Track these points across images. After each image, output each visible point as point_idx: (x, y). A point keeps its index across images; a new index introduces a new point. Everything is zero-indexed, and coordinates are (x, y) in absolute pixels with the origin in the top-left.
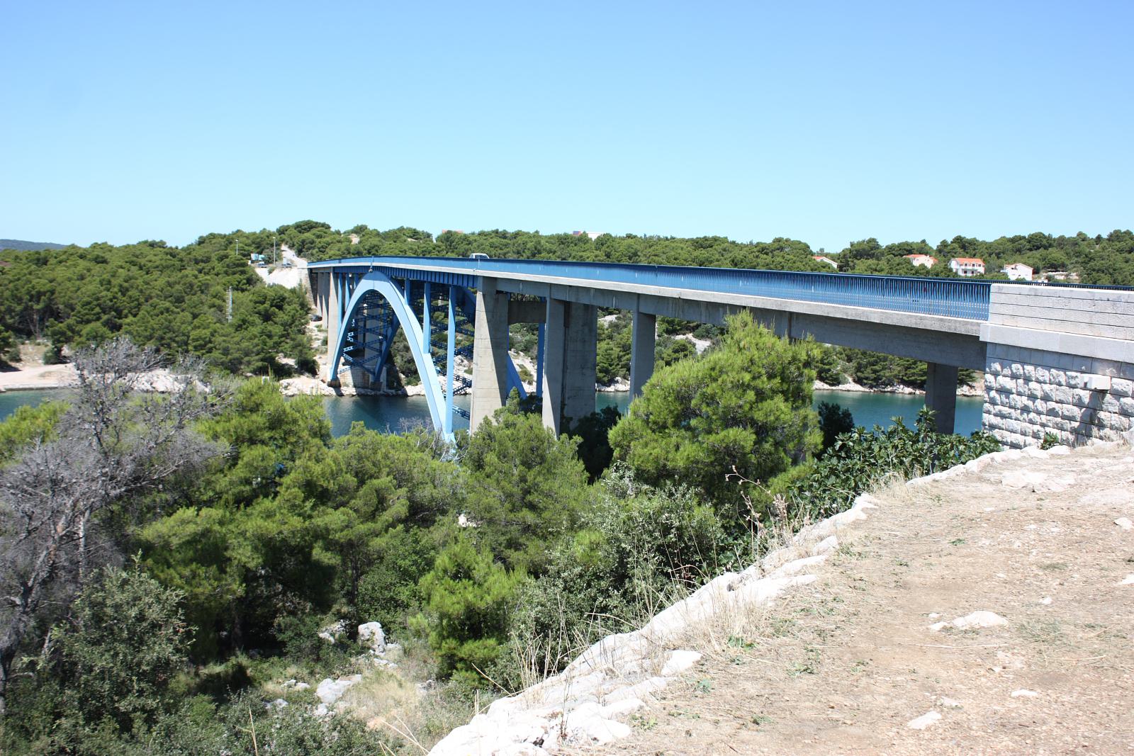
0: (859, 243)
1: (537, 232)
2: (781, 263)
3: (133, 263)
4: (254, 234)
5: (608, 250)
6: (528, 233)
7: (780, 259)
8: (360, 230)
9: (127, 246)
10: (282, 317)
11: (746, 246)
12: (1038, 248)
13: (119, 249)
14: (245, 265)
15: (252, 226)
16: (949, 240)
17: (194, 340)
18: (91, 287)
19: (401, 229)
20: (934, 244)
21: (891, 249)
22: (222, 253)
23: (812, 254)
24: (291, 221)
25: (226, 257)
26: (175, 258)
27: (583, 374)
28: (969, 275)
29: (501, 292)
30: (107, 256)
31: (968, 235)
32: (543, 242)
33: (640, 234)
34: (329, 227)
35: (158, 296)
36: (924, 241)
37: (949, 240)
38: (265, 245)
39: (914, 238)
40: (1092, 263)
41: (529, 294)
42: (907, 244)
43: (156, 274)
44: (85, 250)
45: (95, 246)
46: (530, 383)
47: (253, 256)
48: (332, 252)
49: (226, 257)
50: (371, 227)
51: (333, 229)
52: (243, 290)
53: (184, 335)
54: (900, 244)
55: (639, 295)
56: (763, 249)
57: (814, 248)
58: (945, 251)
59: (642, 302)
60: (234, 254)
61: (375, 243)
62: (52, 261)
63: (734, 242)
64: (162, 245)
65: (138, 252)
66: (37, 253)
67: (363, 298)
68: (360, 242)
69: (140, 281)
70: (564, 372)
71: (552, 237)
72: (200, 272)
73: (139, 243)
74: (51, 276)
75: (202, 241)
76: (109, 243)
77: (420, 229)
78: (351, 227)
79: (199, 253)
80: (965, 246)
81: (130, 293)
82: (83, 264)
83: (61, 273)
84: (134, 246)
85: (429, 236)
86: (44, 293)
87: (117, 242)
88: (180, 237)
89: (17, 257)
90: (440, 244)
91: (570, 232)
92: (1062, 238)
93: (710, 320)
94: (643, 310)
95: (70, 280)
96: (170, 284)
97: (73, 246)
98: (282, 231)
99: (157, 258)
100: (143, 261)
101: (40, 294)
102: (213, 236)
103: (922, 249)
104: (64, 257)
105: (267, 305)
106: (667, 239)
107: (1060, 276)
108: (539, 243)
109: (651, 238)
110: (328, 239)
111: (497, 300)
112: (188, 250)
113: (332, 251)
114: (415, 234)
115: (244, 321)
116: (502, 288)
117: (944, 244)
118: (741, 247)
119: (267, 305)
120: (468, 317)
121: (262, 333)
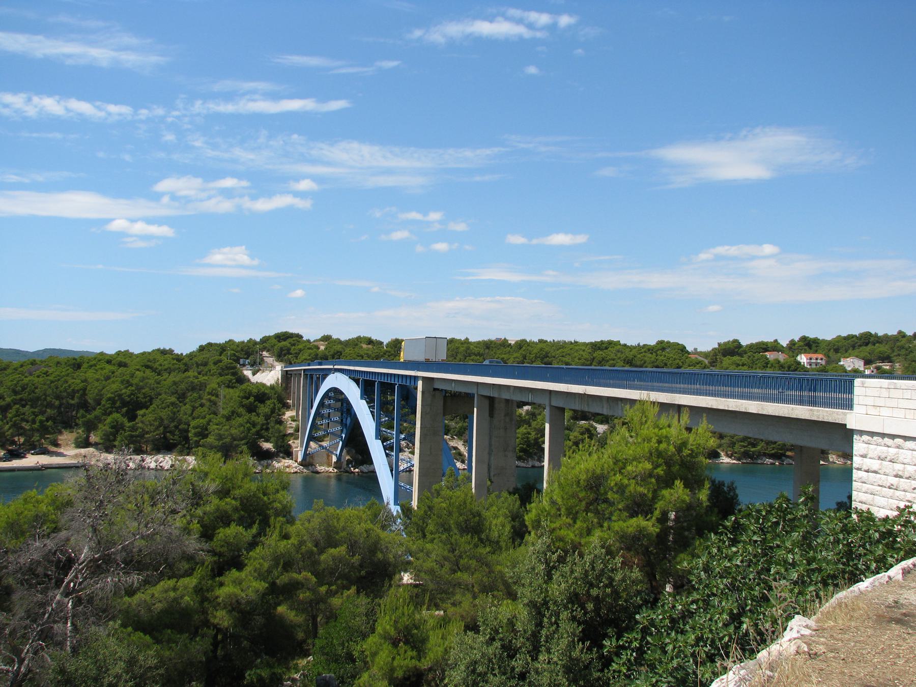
0: (725, 343)
1: (467, 339)
2: (663, 362)
3: (147, 367)
4: (243, 342)
7: (662, 358)
8: (327, 338)
9: (144, 354)
11: (635, 347)
12: (867, 344)
13: (137, 356)
14: (235, 368)
15: (241, 336)
16: (796, 339)
17: (194, 428)
18: (114, 386)
19: (359, 338)
20: (784, 343)
21: (751, 346)
22: (217, 358)
23: (688, 352)
25: (220, 361)
26: (181, 363)
27: (506, 456)
28: (814, 366)
29: (438, 389)
30: (127, 361)
31: (811, 335)
32: (472, 347)
34: (302, 337)
35: (166, 393)
36: (776, 341)
37: (796, 339)
38: (251, 352)
39: (769, 339)
40: (911, 355)
41: (463, 390)
42: (762, 343)
43: (165, 375)
44: (111, 356)
45: (119, 353)
46: (463, 462)
47: (241, 361)
49: (220, 361)
50: (334, 337)
51: (304, 339)
52: (233, 388)
53: (185, 424)
54: (757, 343)
55: (550, 391)
56: (649, 349)
57: (690, 348)
58: (794, 348)
60: (226, 360)
62: (85, 365)
63: (625, 345)
64: (171, 352)
65: (151, 358)
66: (75, 359)
67: (326, 395)
69: (151, 381)
71: (479, 343)
72: (199, 373)
73: (153, 351)
74: (83, 378)
75: (202, 349)
76: (131, 351)
77: (374, 338)
79: (200, 359)
80: (809, 344)
81: (143, 391)
82: (109, 367)
83: (90, 374)
84: (149, 353)
85: (382, 343)
86: (78, 391)
87: (136, 350)
88: (185, 346)
89: (58, 363)
90: (389, 349)
91: (493, 338)
92: (886, 336)
93: (609, 412)
94: (554, 404)
95: (98, 380)
96: (175, 383)
97: (102, 354)
98: (265, 340)
99: (166, 362)
100: (156, 365)
101: (74, 392)
102: (210, 344)
103: (775, 347)
104: (94, 362)
105: (252, 399)
106: (571, 343)
107: (886, 366)
108: (468, 348)
109: (559, 342)
110: (300, 347)
111: (434, 396)
112: (191, 356)
113: (302, 357)
114: (370, 341)
115: (233, 412)
117: (792, 343)
118: (631, 348)
119: (252, 399)
121: (248, 422)
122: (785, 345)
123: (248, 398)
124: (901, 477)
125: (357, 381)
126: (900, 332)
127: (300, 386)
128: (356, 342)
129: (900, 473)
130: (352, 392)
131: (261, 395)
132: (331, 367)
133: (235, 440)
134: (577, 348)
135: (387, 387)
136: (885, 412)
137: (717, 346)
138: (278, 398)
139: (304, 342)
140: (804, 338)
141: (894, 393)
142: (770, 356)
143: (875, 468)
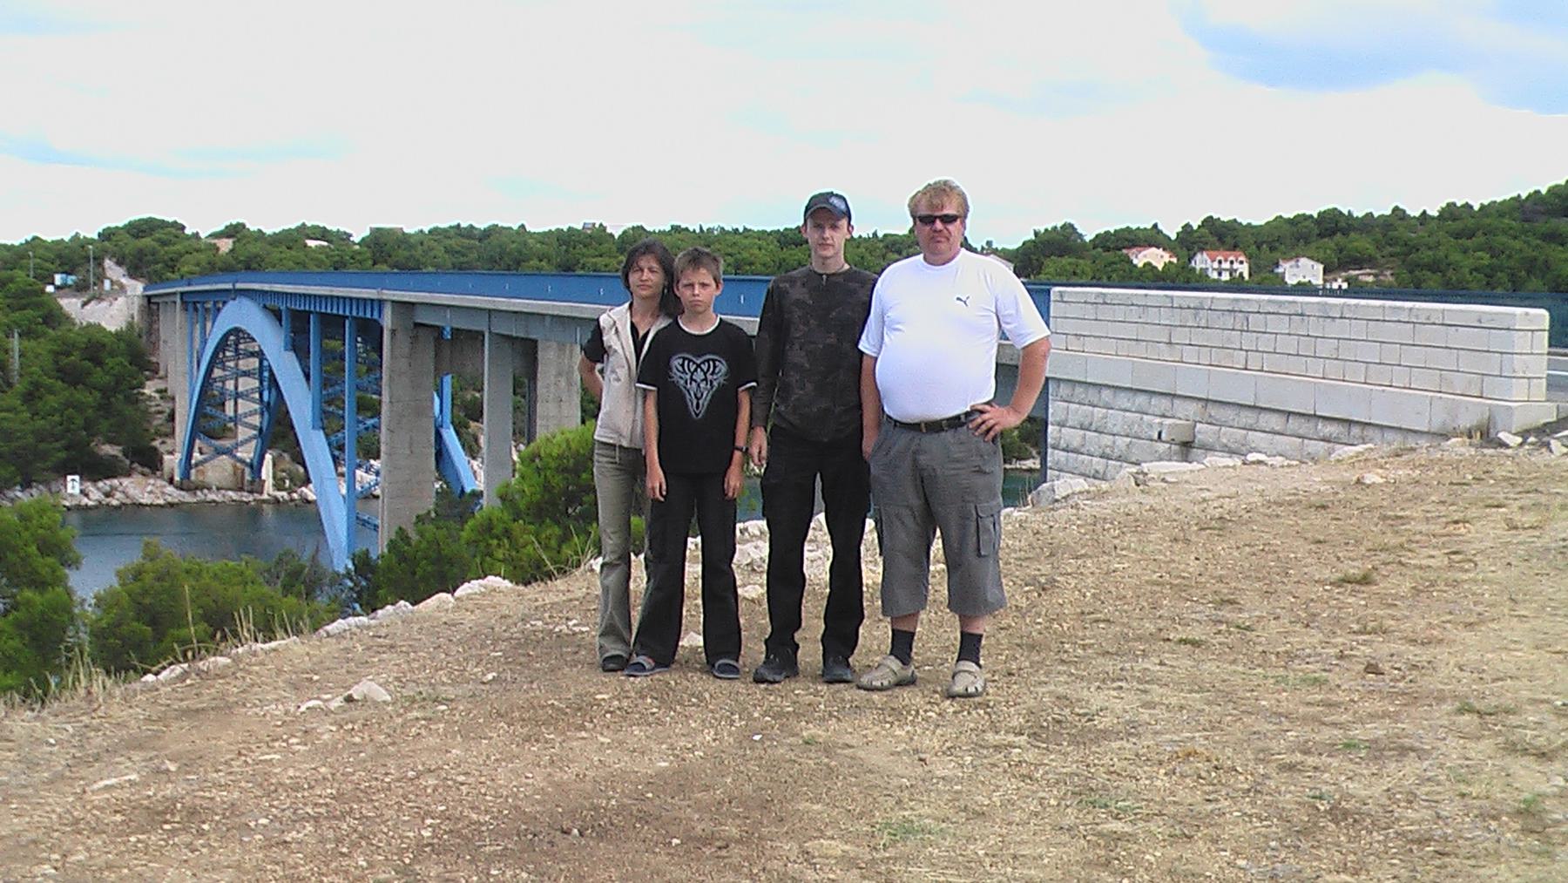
8: (234, 231)
15: (56, 231)
38: (77, 261)
51: (188, 231)
98: (107, 235)
103: (1153, 238)
111: (415, 339)
114: (323, 234)
122: (1088, 239)
123: (68, 354)
124: (1109, 458)
125: (277, 315)
126: (1396, 209)
127: (173, 328)
128: (292, 239)
129: (1108, 451)
130: (270, 338)
131: (96, 346)
132: (229, 286)
133: (42, 441)
134: (746, 242)
135: (332, 324)
136: (1090, 345)
137: (515, 227)
138: (136, 354)
139: (188, 238)
140: (1209, 222)
141: (1106, 312)
142: (1141, 258)
143: (1075, 444)
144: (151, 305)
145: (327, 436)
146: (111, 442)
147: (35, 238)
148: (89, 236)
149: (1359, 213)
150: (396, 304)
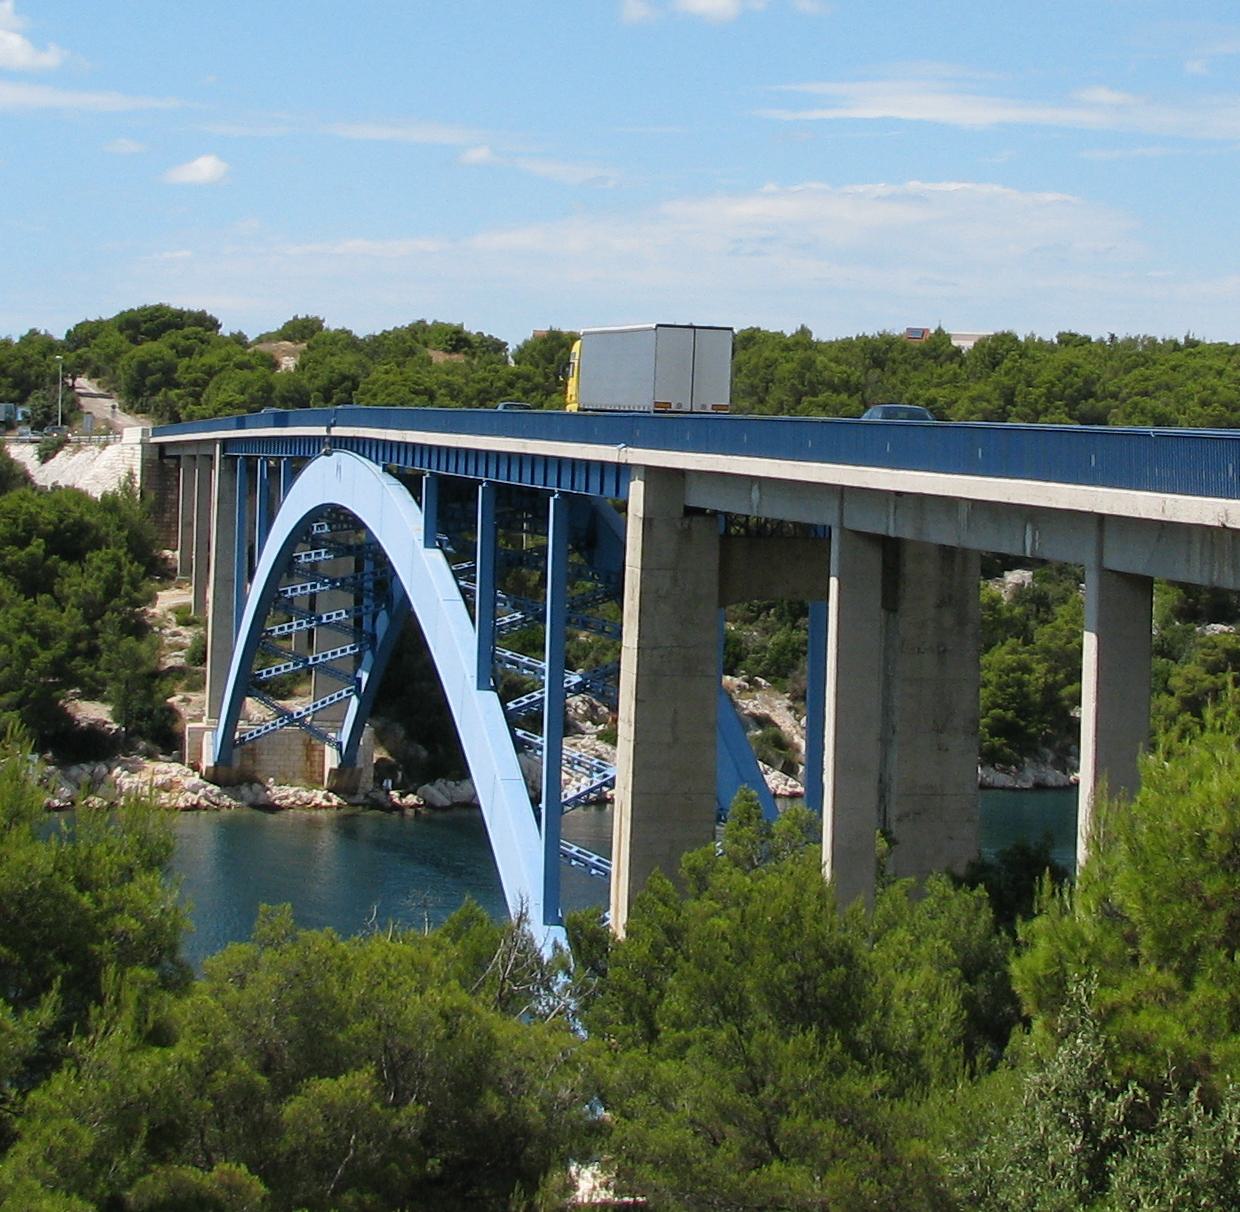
1: (804, 332)
5: (1006, 380)
6: (781, 335)
8: (303, 330)
10: (80, 581)
19: (418, 330)
24: (107, 309)
29: (700, 512)
32: (820, 359)
33: (1097, 332)
34: (214, 325)
46: (789, 769)
48: (222, 397)
50: (332, 324)
51: (225, 331)
59: (1110, 544)
61: (345, 368)
67: (302, 533)
68: (301, 367)
70: (885, 742)
71: (846, 345)
77: (472, 327)
78: (276, 325)
85: (500, 346)
90: (526, 368)
91: (897, 329)
94: (1113, 562)
98: (84, 335)
105: (37, 546)
108: (808, 365)
109: (1131, 343)
110: (211, 359)
111: (686, 535)
114: (458, 340)
116: (698, 498)
119: (37, 546)
120: (607, 581)
123: (23, 543)
128: (407, 344)
130: (397, 522)
131: (72, 531)
132: (321, 431)
135: (519, 503)
138: (124, 545)
144: (161, 464)
145: (503, 701)
146: (91, 694)
147: (33, 333)
148: (1047, 339)
149: (1050, 335)
150: (652, 473)
